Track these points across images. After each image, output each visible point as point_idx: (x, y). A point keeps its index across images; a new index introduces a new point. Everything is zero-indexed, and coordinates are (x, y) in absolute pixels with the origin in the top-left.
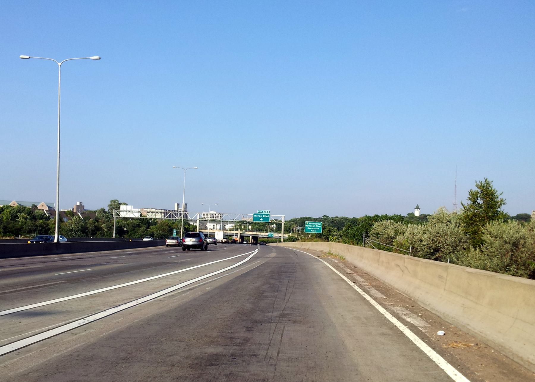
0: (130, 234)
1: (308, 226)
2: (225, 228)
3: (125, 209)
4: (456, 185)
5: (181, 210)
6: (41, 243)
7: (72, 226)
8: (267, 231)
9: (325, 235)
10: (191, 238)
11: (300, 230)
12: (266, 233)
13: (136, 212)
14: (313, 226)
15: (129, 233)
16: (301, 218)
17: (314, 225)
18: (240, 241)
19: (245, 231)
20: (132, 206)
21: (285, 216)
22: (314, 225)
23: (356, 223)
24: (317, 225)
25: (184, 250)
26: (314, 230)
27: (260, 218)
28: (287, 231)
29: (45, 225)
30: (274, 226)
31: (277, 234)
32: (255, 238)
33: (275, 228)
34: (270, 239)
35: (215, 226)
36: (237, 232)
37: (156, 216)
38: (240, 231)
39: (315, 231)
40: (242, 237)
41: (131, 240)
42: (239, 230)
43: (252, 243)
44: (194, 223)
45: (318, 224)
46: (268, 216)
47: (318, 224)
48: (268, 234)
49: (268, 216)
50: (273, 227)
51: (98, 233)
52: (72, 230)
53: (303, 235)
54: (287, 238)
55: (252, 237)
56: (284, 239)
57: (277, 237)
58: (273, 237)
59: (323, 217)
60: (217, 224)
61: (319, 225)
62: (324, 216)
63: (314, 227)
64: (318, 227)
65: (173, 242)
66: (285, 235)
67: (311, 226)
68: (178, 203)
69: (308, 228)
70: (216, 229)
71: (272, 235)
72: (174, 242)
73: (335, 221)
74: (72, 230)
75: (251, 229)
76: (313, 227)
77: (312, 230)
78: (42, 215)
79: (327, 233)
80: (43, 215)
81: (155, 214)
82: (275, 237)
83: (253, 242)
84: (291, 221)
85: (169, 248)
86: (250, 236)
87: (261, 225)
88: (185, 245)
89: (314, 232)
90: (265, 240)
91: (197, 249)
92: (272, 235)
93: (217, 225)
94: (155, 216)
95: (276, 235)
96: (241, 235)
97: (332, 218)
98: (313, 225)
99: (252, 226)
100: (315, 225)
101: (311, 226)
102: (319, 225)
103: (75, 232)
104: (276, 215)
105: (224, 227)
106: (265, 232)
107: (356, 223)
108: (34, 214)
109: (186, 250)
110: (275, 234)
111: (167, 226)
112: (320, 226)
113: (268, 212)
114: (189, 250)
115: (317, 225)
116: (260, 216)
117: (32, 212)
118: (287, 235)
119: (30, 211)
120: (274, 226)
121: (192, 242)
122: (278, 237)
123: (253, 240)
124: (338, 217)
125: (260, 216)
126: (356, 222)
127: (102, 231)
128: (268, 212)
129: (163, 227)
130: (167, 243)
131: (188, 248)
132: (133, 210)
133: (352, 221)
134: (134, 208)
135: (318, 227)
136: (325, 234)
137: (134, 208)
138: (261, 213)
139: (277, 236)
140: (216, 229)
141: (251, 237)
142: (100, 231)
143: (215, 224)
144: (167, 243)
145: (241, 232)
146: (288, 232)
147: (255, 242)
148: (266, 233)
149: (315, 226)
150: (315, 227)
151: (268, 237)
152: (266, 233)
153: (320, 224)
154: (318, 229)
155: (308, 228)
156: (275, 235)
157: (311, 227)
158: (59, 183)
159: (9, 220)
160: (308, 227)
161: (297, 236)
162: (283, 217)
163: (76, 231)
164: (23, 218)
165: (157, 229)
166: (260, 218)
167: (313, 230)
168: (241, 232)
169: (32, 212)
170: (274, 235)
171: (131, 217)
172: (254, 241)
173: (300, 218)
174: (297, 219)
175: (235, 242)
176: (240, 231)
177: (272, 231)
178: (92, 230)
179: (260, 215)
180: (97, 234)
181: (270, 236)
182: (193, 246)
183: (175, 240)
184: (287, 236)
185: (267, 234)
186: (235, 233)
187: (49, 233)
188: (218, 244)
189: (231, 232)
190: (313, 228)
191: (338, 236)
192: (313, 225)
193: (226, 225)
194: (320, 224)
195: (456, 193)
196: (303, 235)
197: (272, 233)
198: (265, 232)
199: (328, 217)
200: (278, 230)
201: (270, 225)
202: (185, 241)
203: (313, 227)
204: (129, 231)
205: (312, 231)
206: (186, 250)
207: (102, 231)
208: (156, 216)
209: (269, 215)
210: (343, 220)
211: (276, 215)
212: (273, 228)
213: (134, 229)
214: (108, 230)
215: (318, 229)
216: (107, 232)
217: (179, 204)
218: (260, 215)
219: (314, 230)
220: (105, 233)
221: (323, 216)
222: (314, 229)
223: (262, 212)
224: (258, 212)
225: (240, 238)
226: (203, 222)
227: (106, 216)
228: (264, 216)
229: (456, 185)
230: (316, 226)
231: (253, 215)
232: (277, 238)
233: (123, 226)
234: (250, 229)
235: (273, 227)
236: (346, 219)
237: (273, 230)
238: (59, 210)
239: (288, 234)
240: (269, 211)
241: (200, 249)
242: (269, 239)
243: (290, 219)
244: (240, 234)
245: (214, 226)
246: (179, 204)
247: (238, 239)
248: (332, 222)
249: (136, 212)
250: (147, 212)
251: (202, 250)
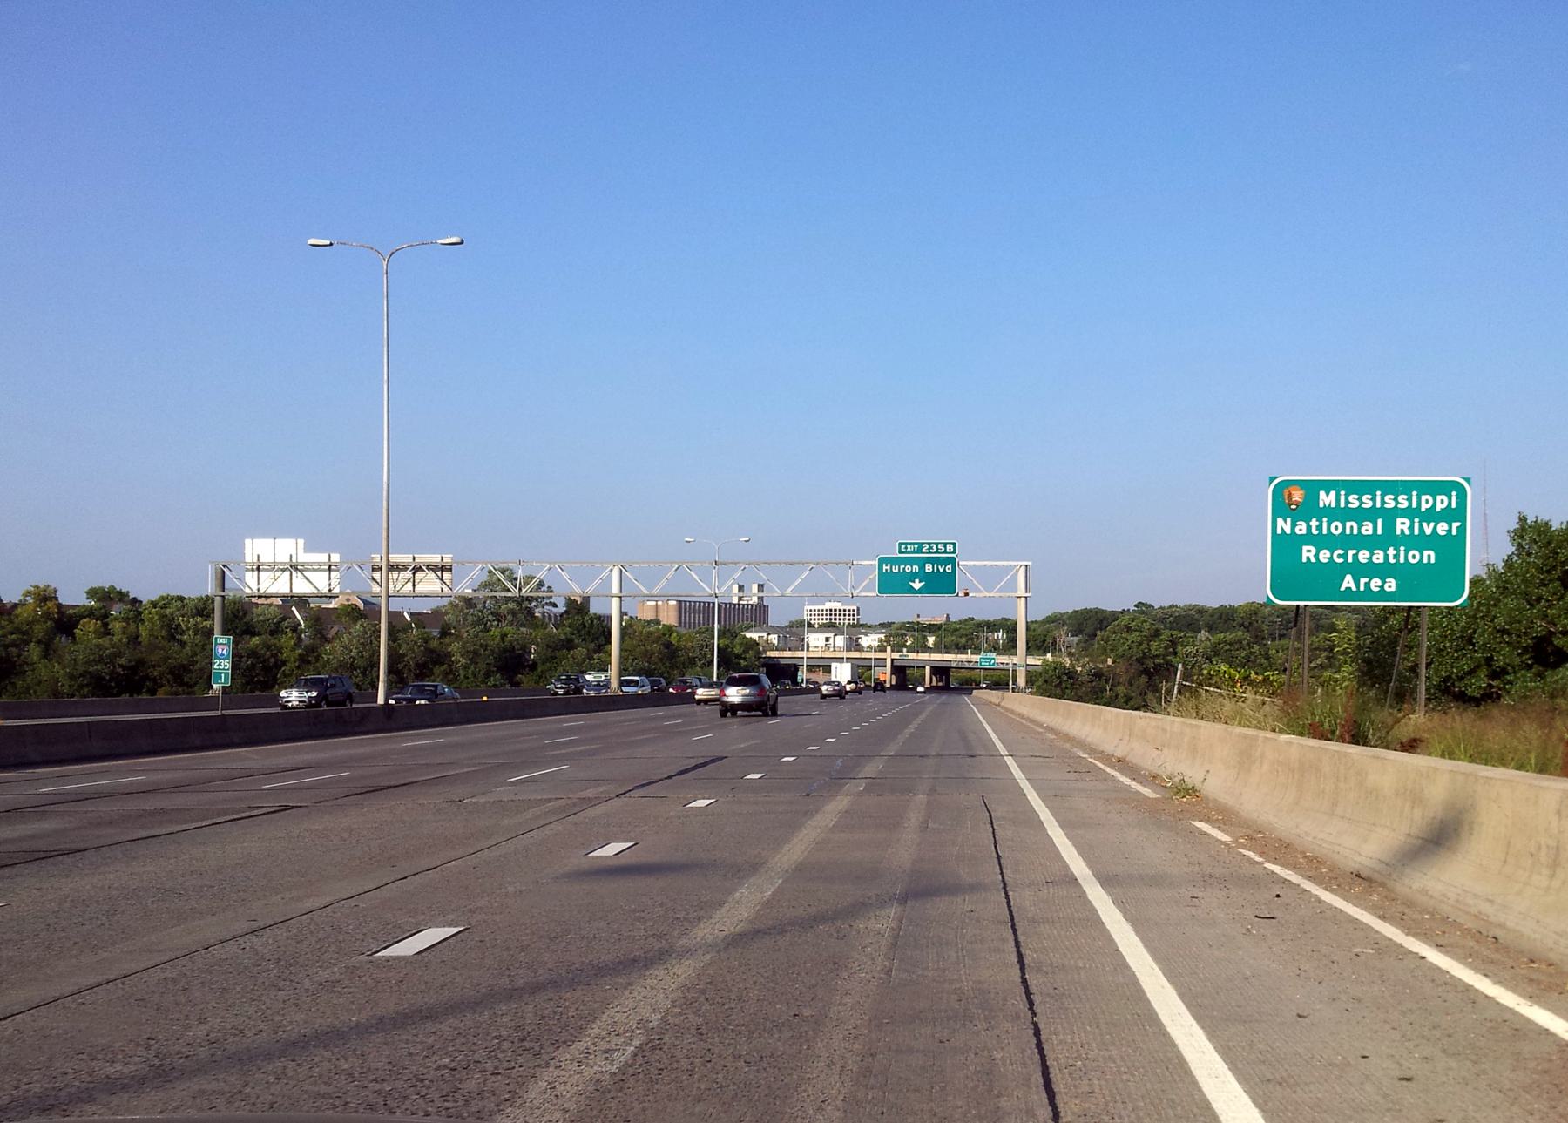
0: (542, 671)
1: (1301, 528)
2: (859, 645)
3: (266, 558)
4: (1487, 512)
5: (748, 601)
6: (417, 702)
7: (352, 654)
8: (977, 651)
9: (1157, 656)
10: (740, 688)
11: (1075, 645)
12: (972, 654)
13: (317, 567)
14: (1367, 528)
15: (540, 670)
16: (1075, 612)
17: (1371, 514)
18: (894, 683)
19: (908, 652)
20: (301, 542)
21: (1030, 563)
22: (1371, 514)
23: (1234, 621)
24: (1411, 513)
25: (723, 714)
26: (1383, 571)
27: (913, 576)
28: (1039, 648)
29: (268, 653)
30: (1000, 634)
31: (1006, 657)
32: (941, 672)
33: (1004, 641)
34: (986, 673)
35: (831, 641)
36: (880, 655)
37: (414, 586)
38: (893, 651)
39: (1391, 585)
40: (899, 670)
41: (485, 699)
42: (889, 648)
43: (932, 689)
44: (769, 634)
45: (1426, 502)
46: (949, 568)
47: (1426, 502)
48: (979, 657)
49: (949, 568)
50: (998, 637)
51: (438, 670)
52: (352, 664)
53: (1087, 659)
54: (1040, 669)
55: (932, 667)
56: (1027, 671)
57: (1006, 667)
58: (996, 667)
59: (1136, 606)
60: (835, 635)
61: (1431, 515)
62: (1140, 603)
63: (1371, 543)
64: (1420, 542)
65: (712, 693)
66: (1031, 660)
67: (1336, 528)
68: (741, 584)
69: (1308, 553)
70: (834, 647)
71: (993, 661)
72: (714, 693)
73: (1171, 616)
74: (352, 664)
75: (935, 644)
76: (1360, 542)
77: (1358, 570)
78: (275, 621)
79: (1166, 648)
80: (279, 622)
81: (408, 574)
82: (1001, 666)
83: (934, 683)
84: (1048, 620)
85: (702, 707)
86: (924, 667)
87: (964, 633)
88: (725, 704)
89: (1382, 594)
90: (973, 678)
91: (753, 713)
92: (993, 661)
93: (837, 637)
94: (410, 583)
95: (1004, 659)
96: (896, 663)
97: (1161, 608)
98: (1360, 515)
99: (938, 637)
100: (1390, 516)
101: (1336, 528)
102: (1431, 515)
103: (361, 673)
104: (988, 563)
105: (857, 641)
106: (969, 651)
107: (1234, 621)
108: (248, 617)
109: (729, 714)
110: (999, 657)
111: (657, 643)
112: (1442, 528)
113: (950, 548)
114: (734, 714)
115: (1411, 513)
116: (908, 569)
117: (241, 614)
118: (1040, 659)
119: (238, 610)
120: (1001, 636)
121: (743, 696)
122: (1011, 665)
123: (934, 678)
124: (1176, 606)
125: (908, 569)
126: (1232, 616)
127: (450, 666)
128: (950, 548)
129: (644, 645)
130: (697, 697)
131: (729, 710)
132: (304, 558)
133: (1221, 615)
134: (308, 549)
135: (1420, 542)
136: (1158, 652)
137: (308, 549)
138: (914, 552)
139: (1007, 664)
140: (834, 647)
141: (928, 669)
142: (445, 666)
143: (832, 635)
144: (697, 697)
145: (896, 655)
146: (1041, 651)
147: (940, 684)
148: (973, 656)
149: (1390, 526)
150: (1388, 539)
151: (979, 666)
152: (972, 654)
153: (1442, 502)
154: (1430, 555)
155: (1308, 553)
156: (1003, 661)
157: (1346, 541)
158: (388, 536)
159: (157, 638)
160: (1309, 539)
161: (1069, 662)
162: (1023, 568)
163: (365, 669)
164: (196, 632)
165: (626, 653)
166: (913, 576)
167: (1371, 570)
168: (896, 655)
169: (241, 614)
170: (999, 661)
171: (295, 591)
172: (937, 682)
173: (1070, 611)
174: (1062, 615)
175: (879, 686)
176: (893, 651)
177: (994, 648)
178: (417, 665)
179: (911, 561)
180: (433, 674)
181: (985, 664)
182: (742, 706)
183: (716, 690)
184: (1039, 663)
185: (975, 658)
186: (873, 657)
187: (279, 676)
188: (847, 697)
189: (781, 656)
190: (1363, 556)
191: (1200, 659)
192: (1360, 515)
193: (863, 636)
194: (1442, 502)
195: (1486, 534)
196: (1087, 659)
197: (993, 655)
198: (969, 651)
199: (1151, 606)
200: (1010, 647)
201: (988, 633)
202: (725, 695)
203: (1360, 542)
204: (539, 662)
205: (1348, 582)
206: (729, 714)
207: (450, 666)
208: (414, 586)
209: (952, 561)
210: (1191, 612)
211: (988, 563)
212: (997, 642)
213: (553, 654)
214: (470, 660)
215: (1430, 555)
216: (466, 668)
217: (743, 586)
218: (911, 561)
219: (1383, 571)
220: (461, 672)
221: (1136, 603)
222: (1379, 557)
223: (920, 551)
224: (901, 552)
225: (892, 674)
226: (795, 631)
227: (475, 619)
228: (929, 568)
229: (1485, 514)
230: (1402, 525)
231: (876, 563)
232: (1009, 670)
233: (517, 647)
234: (931, 646)
235: (998, 637)
236: (1201, 611)
237: (997, 646)
238: (390, 610)
239: (1042, 658)
240: (954, 544)
241: (760, 713)
242: (986, 674)
243: (1044, 617)
244: (892, 660)
245: (827, 639)
246: (743, 586)
247: (887, 677)
248: (1164, 619)
249: (317, 567)
250: (373, 570)
251: (765, 714)
